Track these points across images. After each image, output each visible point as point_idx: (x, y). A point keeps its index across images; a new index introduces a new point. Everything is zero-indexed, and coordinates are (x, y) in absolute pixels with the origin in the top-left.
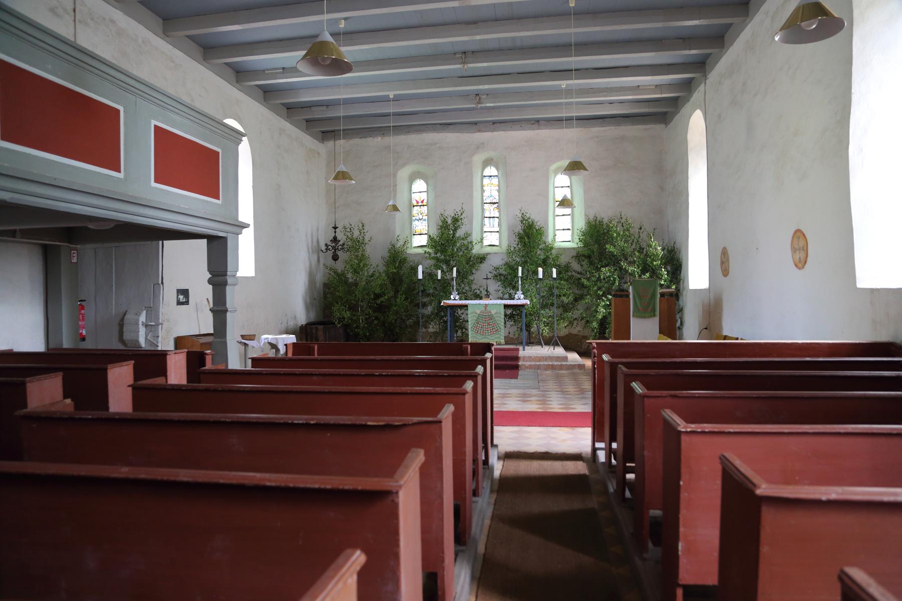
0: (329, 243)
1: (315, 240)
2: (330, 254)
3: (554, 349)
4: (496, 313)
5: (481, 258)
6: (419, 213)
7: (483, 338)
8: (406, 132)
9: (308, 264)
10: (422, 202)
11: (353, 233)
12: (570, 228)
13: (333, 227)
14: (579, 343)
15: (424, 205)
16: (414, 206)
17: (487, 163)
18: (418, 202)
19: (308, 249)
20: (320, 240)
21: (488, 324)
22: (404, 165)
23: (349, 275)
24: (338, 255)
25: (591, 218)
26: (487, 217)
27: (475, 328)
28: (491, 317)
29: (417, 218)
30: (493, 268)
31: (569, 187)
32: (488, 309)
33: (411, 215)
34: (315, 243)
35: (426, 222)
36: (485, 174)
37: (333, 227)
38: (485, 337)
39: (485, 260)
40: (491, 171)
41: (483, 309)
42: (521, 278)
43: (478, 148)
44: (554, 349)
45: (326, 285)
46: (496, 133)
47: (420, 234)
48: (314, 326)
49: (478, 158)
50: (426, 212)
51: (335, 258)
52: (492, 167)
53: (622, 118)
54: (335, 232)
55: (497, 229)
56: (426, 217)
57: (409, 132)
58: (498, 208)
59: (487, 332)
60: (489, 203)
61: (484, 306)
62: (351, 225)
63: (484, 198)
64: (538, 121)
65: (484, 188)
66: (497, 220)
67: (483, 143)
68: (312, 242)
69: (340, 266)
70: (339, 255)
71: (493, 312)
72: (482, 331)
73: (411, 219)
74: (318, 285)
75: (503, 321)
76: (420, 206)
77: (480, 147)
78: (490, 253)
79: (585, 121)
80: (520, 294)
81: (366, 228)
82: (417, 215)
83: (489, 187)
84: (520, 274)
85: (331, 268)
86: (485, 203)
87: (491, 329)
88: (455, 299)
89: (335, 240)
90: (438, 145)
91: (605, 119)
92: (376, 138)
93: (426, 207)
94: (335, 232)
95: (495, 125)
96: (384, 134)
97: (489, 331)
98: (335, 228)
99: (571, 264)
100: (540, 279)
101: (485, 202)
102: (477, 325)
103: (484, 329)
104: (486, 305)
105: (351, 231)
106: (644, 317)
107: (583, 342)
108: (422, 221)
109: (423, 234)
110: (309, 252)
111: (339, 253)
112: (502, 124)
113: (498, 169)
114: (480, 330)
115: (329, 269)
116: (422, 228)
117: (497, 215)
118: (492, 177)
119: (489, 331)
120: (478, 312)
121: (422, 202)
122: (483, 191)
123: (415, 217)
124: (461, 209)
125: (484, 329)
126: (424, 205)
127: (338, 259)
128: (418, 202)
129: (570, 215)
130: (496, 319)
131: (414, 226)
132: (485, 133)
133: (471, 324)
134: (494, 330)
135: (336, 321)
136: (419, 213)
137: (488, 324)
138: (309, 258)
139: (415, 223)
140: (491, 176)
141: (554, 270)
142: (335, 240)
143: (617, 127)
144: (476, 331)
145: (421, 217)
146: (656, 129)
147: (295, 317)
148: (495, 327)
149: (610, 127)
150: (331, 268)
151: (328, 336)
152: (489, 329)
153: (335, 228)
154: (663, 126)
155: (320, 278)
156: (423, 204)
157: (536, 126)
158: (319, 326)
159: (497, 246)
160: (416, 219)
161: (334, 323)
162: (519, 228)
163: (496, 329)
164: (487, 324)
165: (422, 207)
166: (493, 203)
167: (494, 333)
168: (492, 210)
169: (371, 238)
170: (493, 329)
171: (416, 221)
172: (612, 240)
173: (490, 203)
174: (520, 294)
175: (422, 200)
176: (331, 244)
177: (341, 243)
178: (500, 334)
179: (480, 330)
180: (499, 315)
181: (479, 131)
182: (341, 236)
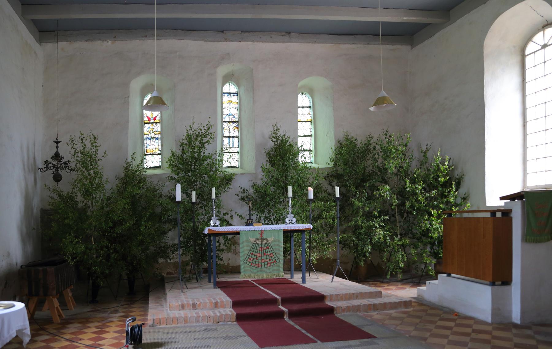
0: (50, 160)
1: (31, 156)
2: (50, 174)
3: (310, 276)
4: (275, 241)
5: (227, 180)
6: (151, 132)
7: (258, 271)
8: (142, 37)
9: (23, 184)
10: (155, 119)
11: (85, 145)
12: (313, 149)
13: (55, 142)
14: (330, 267)
15: (156, 123)
16: (145, 123)
17: (227, 79)
18: (149, 119)
19: (24, 165)
20: (36, 157)
21: (265, 254)
22: (138, 74)
23: (79, 198)
24: (60, 175)
25: (341, 138)
26: (226, 137)
27: (249, 260)
28: (268, 246)
29: (149, 136)
30: (242, 190)
31: (310, 107)
32: (265, 236)
33: (143, 134)
34: (32, 161)
35: (160, 141)
36: (224, 91)
37: (55, 142)
38: (261, 271)
39: (231, 181)
40: (230, 88)
41: (258, 236)
42: (291, 198)
43: (223, 58)
44: (310, 276)
45: (43, 212)
46: (242, 44)
47: (152, 155)
48: (41, 268)
49: (222, 70)
50: (159, 130)
51: (57, 178)
52: (231, 84)
53: (372, 36)
54: (57, 147)
55: (237, 150)
56: (160, 136)
57: (146, 36)
58: (237, 127)
59: (263, 264)
60: (228, 122)
61: (260, 233)
62: (83, 135)
63: (224, 116)
64: (289, 33)
65: (224, 106)
66: (236, 139)
67: (228, 54)
68: (28, 158)
69: (65, 187)
70: (63, 176)
71: (270, 240)
72: (257, 263)
73: (143, 137)
74: (35, 211)
75: (282, 249)
76: (152, 123)
77: (225, 58)
78: (237, 174)
79: (337, 36)
80: (290, 218)
81: (99, 142)
82: (148, 133)
83: (228, 105)
84: (290, 194)
85: (54, 190)
86: (224, 122)
87: (268, 260)
88: (215, 226)
89: (57, 156)
90: (178, 54)
91: (356, 36)
92: (105, 42)
93: (159, 125)
94: (57, 147)
95: (243, 34)
96: (115, 37)
97: (266, 263)
98: (57, 142)
99: (322, 185)
100: (311, 200)
101: (224, 120)
102: (251, 255)
103: (260, 261)
104: (262, 232)
105: (82, 142)
106: (540, 241)
107: (334, 266)
108: (154, 140)
109: (155, 154)
110: (24, 169)
111: (62, 173)
112: (251, 34)
113: (238, 85)
114: (254, 262)
115: (52, 190)
116: (153, 147)
117: (236, 134)
118: (232, 95)
119: (266, 263)
120: (252, 240)
121: (155, 119)
122: (222, 109)
123: (147, 136)
124: (207, 123)
125: (260, 261)
126: (156, 123)
127: (61, 178)
128: (149, 119)
129: (311, 136)
130: (274, 248)
131: (146, 145)
132: (232, 43)
133: (244, 255)
134: (271, 261)
135: (68, 258)
136: (151, 132)
137: (265, 254)
138: (25, 178)
139: (147, 142)
140: (230, 93)
141: (311, 189)
142: (57, 156)
143: (366, 46)
144: (250, 264)
145: (153, 135)
146: (403, 49)
147: (9, 254)
148: (273, 257)
149: (359, 45)
150: (54, 190)
151: (60, 280)
152: (266, 260)
153: (57, 142)
154: (409, 47)
155: (36, 203)
156: (155, 121)
157: (287, 38)
158: (48, 268)
159: (236, 167)
160: (147, 138)
161: (66, 261)
162: (271, 144)
163: (274, 260)
164: (263, 255)
165: (154, 124)
166: (232, 122)
167: (272, 264)
168: (231, 130)
169: (105, 153)
170: (270, 260)
171: (148, 140)
172: (64, 202)
173: (229, 122)
174: (290, 218)
175: (154, 117)
176: (52, 162)
177: (64, 160)
178: (279, 266)
179: (254, 262)
180: (278, 243)
181: (226, 40)
182: (66, 152)
